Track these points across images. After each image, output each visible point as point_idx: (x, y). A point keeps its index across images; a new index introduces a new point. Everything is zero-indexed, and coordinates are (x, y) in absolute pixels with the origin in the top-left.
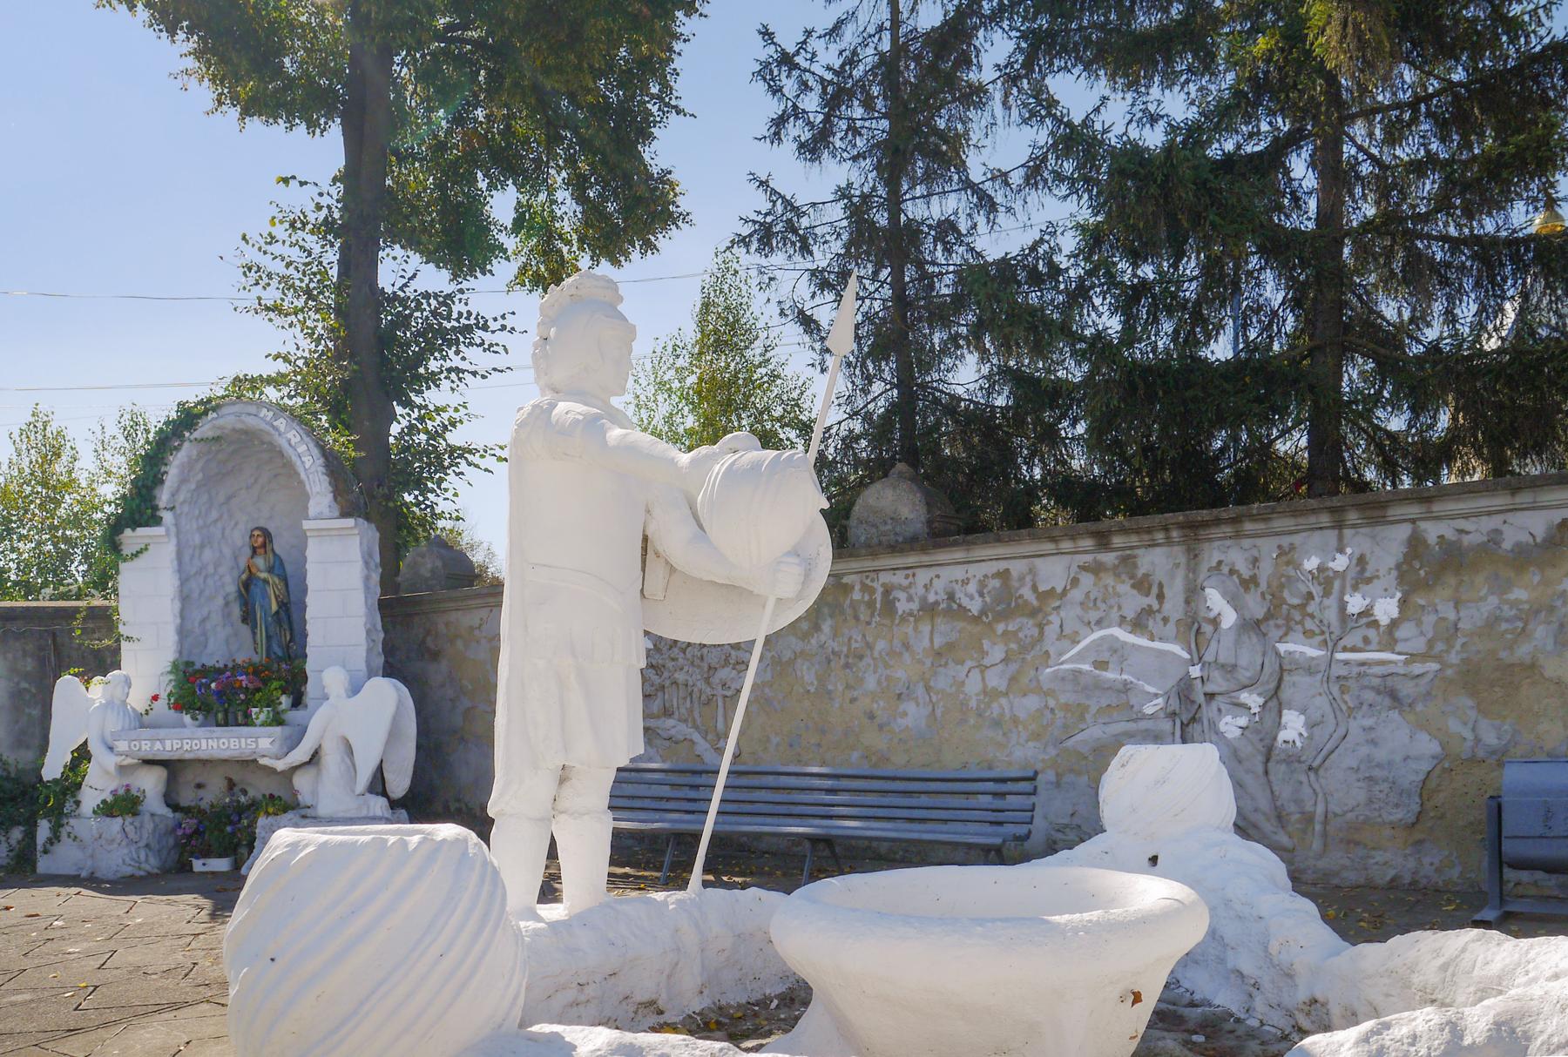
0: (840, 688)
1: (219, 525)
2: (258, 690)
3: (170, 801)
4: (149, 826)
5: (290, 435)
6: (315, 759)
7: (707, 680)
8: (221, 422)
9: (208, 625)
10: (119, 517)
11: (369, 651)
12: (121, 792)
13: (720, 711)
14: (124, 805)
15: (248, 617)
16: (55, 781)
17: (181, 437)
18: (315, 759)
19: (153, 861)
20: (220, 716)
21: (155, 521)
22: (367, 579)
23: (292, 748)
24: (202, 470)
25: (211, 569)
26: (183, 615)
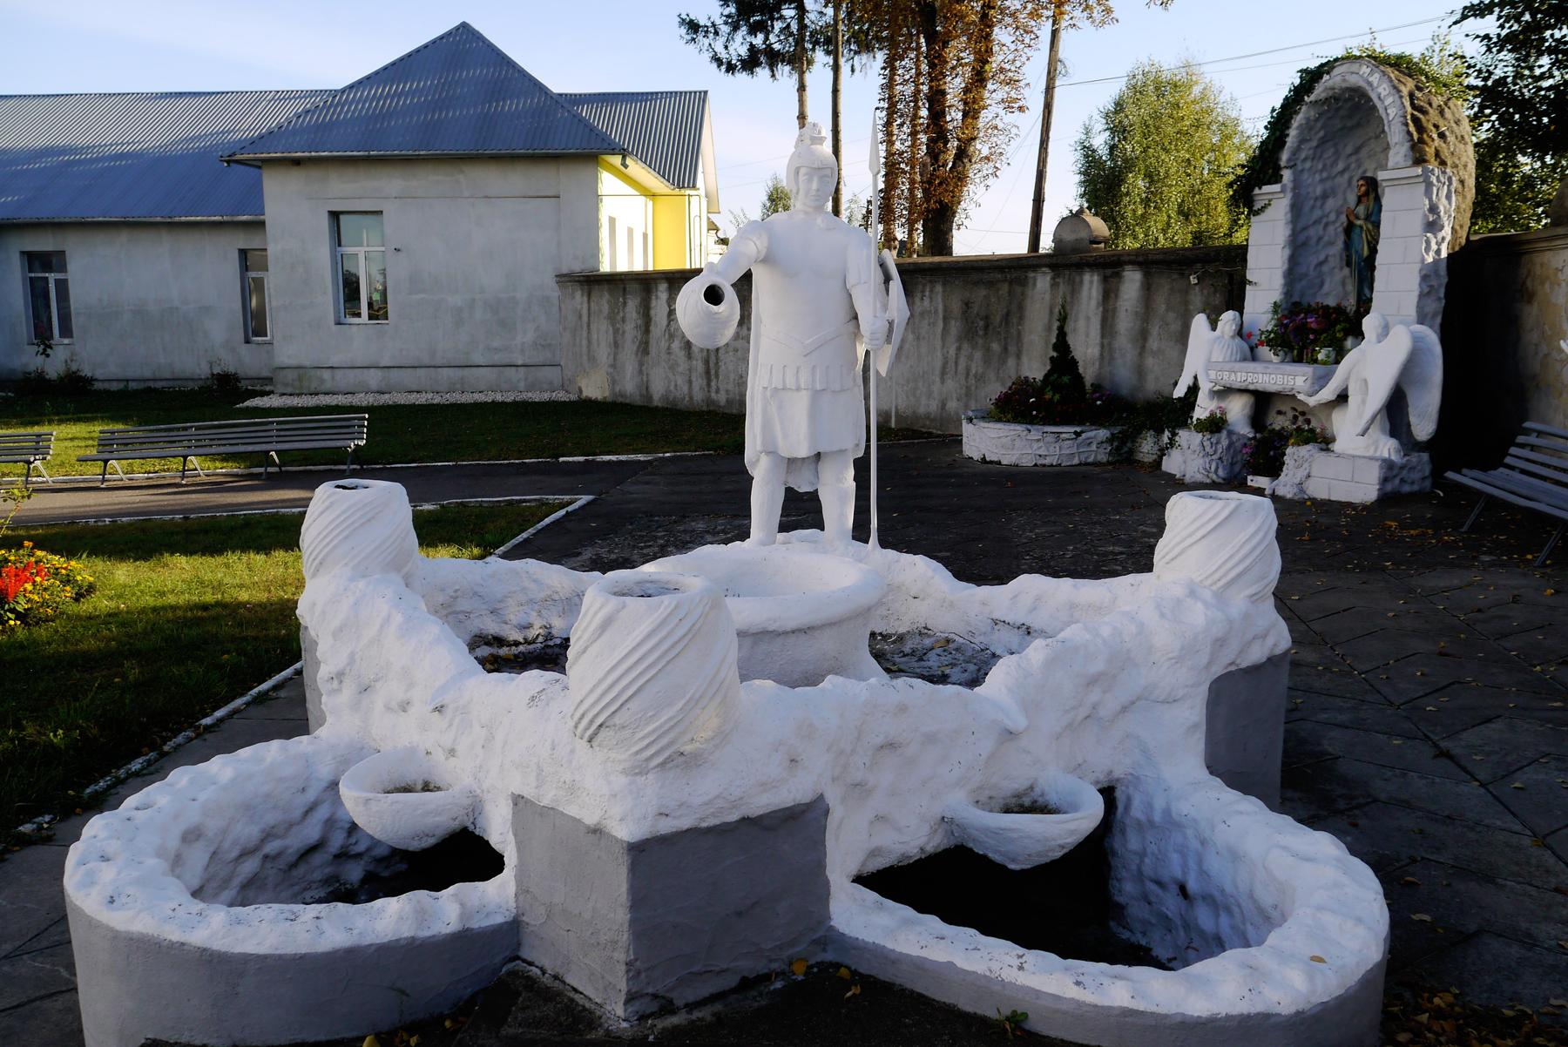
1: (1346, 176)
4: (1225, 443)
5: (1380, 90)
6: (1342, 398)
8: (1330, 83)
9: (1325, 268)
14: (1215, 425)
18: (1342, 398)
21: (1277, 179)
23: (1322, 387)
24: (1323, 127)
26: (1293, 261)
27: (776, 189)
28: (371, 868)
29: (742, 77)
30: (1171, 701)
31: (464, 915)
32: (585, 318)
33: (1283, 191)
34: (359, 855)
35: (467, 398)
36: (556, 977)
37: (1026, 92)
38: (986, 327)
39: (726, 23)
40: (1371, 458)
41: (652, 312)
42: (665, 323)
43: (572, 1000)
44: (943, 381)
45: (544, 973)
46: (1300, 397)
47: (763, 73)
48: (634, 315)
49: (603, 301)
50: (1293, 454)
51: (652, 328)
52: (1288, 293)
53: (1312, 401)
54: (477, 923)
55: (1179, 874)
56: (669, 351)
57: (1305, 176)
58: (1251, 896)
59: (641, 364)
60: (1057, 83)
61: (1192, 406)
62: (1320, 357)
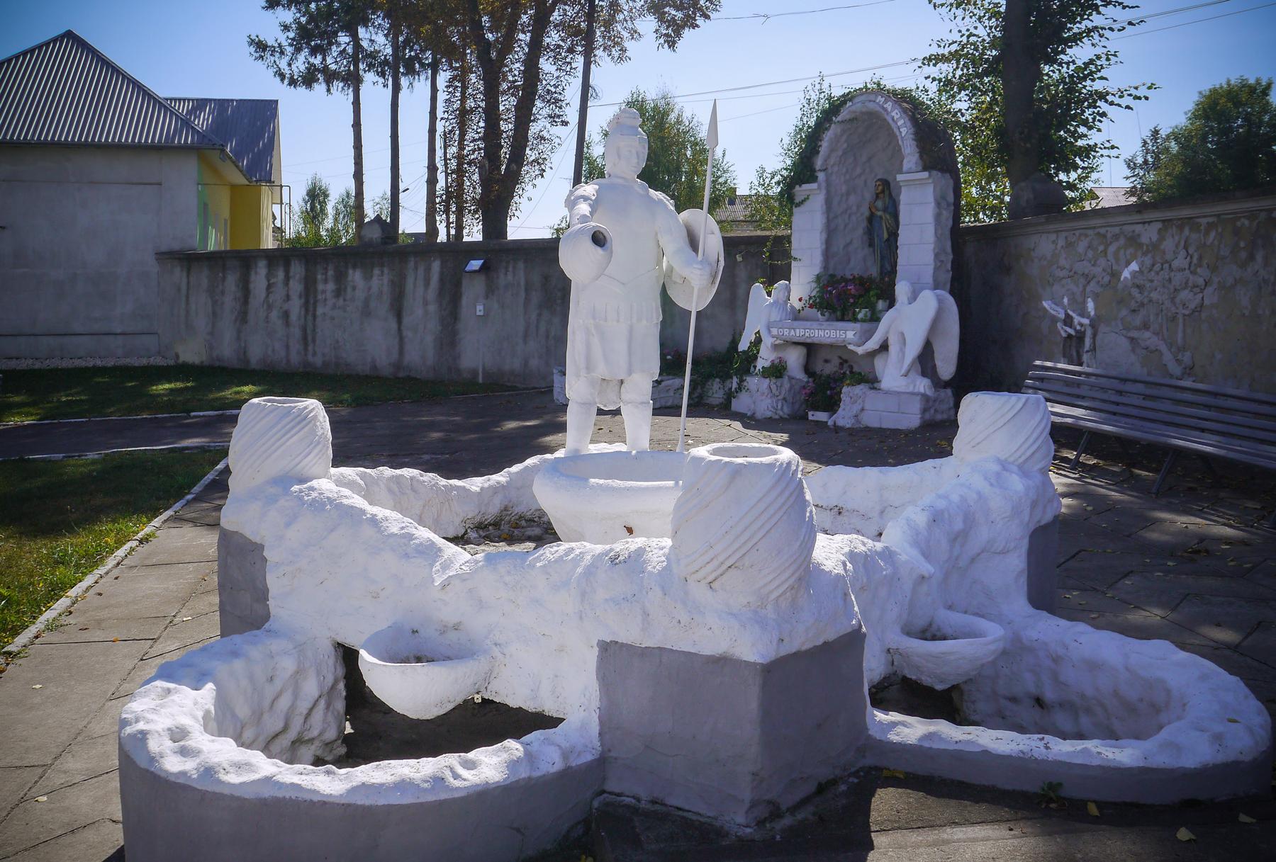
0: (1267, 312)
2: (861, 296)
3: (807, 369)
4: (787, 386)
6: (884, 347)
7: (1173, 300)
8: (853, 108)
10: (792, 178)
11: (936, 269)
12: (777, 362)
13: (1181, 325)
14: (776, 371)
15: (871, 245)
16: (744, 352)
17: (830, 121)
18: (884, 347)
19: (786, 410)
20: (839, 313)
21: (813, 179)
22: (938, 217)
25: (854, 208)
26: (828, 243)
27: (314, 188)
28: (319, 753)
29: (302, 90)
30: (1004, 552)
31: (565, 755)
32: (184, 291)
33: (819, 188)
34: (311, 740)
35: (65, 364)
36: (654, 802)
37: (567, 110)
39: (291, 45)
40: (913, 394)
41: (252, 286)
42: (263, 295)
43: (683, 817)
44: (525, 342)
45: (639, 800)
46: (851, 347)
47: (320, 87)
48: (233, 288)
49: (203, 277)
50: (847, 392)
51: (251, 300)
52: (825, 268)
53: (860, 350)
54: (575, 762)
55: (1033, 690)
56: (267, 320)
57: (834, 177)
58: (1116, 694)
59: (239, 332)
60: (589, 104)
61: (755, 358)
62: (860, 316)
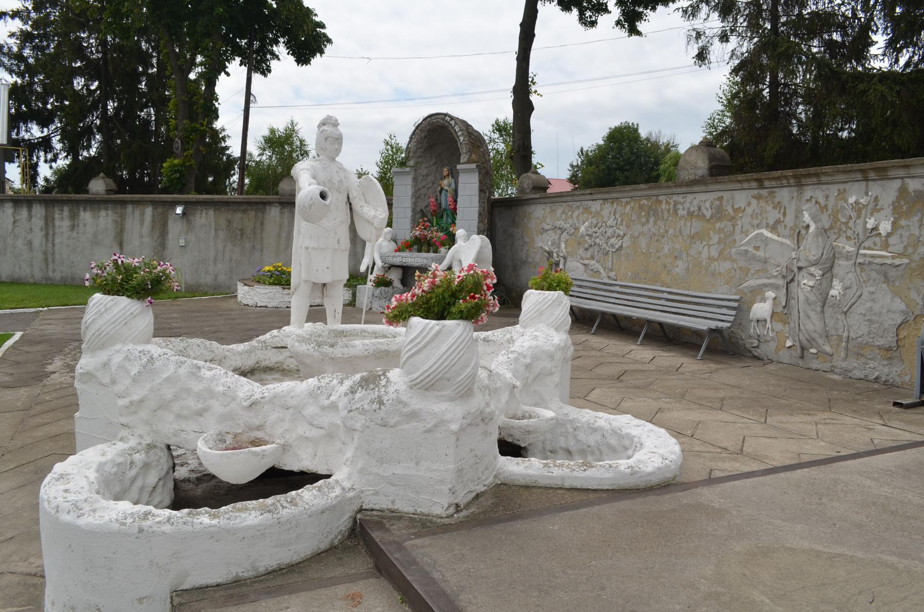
30: (551, 374)
38: (242, 235)
